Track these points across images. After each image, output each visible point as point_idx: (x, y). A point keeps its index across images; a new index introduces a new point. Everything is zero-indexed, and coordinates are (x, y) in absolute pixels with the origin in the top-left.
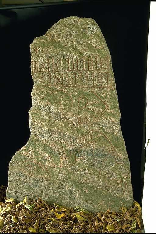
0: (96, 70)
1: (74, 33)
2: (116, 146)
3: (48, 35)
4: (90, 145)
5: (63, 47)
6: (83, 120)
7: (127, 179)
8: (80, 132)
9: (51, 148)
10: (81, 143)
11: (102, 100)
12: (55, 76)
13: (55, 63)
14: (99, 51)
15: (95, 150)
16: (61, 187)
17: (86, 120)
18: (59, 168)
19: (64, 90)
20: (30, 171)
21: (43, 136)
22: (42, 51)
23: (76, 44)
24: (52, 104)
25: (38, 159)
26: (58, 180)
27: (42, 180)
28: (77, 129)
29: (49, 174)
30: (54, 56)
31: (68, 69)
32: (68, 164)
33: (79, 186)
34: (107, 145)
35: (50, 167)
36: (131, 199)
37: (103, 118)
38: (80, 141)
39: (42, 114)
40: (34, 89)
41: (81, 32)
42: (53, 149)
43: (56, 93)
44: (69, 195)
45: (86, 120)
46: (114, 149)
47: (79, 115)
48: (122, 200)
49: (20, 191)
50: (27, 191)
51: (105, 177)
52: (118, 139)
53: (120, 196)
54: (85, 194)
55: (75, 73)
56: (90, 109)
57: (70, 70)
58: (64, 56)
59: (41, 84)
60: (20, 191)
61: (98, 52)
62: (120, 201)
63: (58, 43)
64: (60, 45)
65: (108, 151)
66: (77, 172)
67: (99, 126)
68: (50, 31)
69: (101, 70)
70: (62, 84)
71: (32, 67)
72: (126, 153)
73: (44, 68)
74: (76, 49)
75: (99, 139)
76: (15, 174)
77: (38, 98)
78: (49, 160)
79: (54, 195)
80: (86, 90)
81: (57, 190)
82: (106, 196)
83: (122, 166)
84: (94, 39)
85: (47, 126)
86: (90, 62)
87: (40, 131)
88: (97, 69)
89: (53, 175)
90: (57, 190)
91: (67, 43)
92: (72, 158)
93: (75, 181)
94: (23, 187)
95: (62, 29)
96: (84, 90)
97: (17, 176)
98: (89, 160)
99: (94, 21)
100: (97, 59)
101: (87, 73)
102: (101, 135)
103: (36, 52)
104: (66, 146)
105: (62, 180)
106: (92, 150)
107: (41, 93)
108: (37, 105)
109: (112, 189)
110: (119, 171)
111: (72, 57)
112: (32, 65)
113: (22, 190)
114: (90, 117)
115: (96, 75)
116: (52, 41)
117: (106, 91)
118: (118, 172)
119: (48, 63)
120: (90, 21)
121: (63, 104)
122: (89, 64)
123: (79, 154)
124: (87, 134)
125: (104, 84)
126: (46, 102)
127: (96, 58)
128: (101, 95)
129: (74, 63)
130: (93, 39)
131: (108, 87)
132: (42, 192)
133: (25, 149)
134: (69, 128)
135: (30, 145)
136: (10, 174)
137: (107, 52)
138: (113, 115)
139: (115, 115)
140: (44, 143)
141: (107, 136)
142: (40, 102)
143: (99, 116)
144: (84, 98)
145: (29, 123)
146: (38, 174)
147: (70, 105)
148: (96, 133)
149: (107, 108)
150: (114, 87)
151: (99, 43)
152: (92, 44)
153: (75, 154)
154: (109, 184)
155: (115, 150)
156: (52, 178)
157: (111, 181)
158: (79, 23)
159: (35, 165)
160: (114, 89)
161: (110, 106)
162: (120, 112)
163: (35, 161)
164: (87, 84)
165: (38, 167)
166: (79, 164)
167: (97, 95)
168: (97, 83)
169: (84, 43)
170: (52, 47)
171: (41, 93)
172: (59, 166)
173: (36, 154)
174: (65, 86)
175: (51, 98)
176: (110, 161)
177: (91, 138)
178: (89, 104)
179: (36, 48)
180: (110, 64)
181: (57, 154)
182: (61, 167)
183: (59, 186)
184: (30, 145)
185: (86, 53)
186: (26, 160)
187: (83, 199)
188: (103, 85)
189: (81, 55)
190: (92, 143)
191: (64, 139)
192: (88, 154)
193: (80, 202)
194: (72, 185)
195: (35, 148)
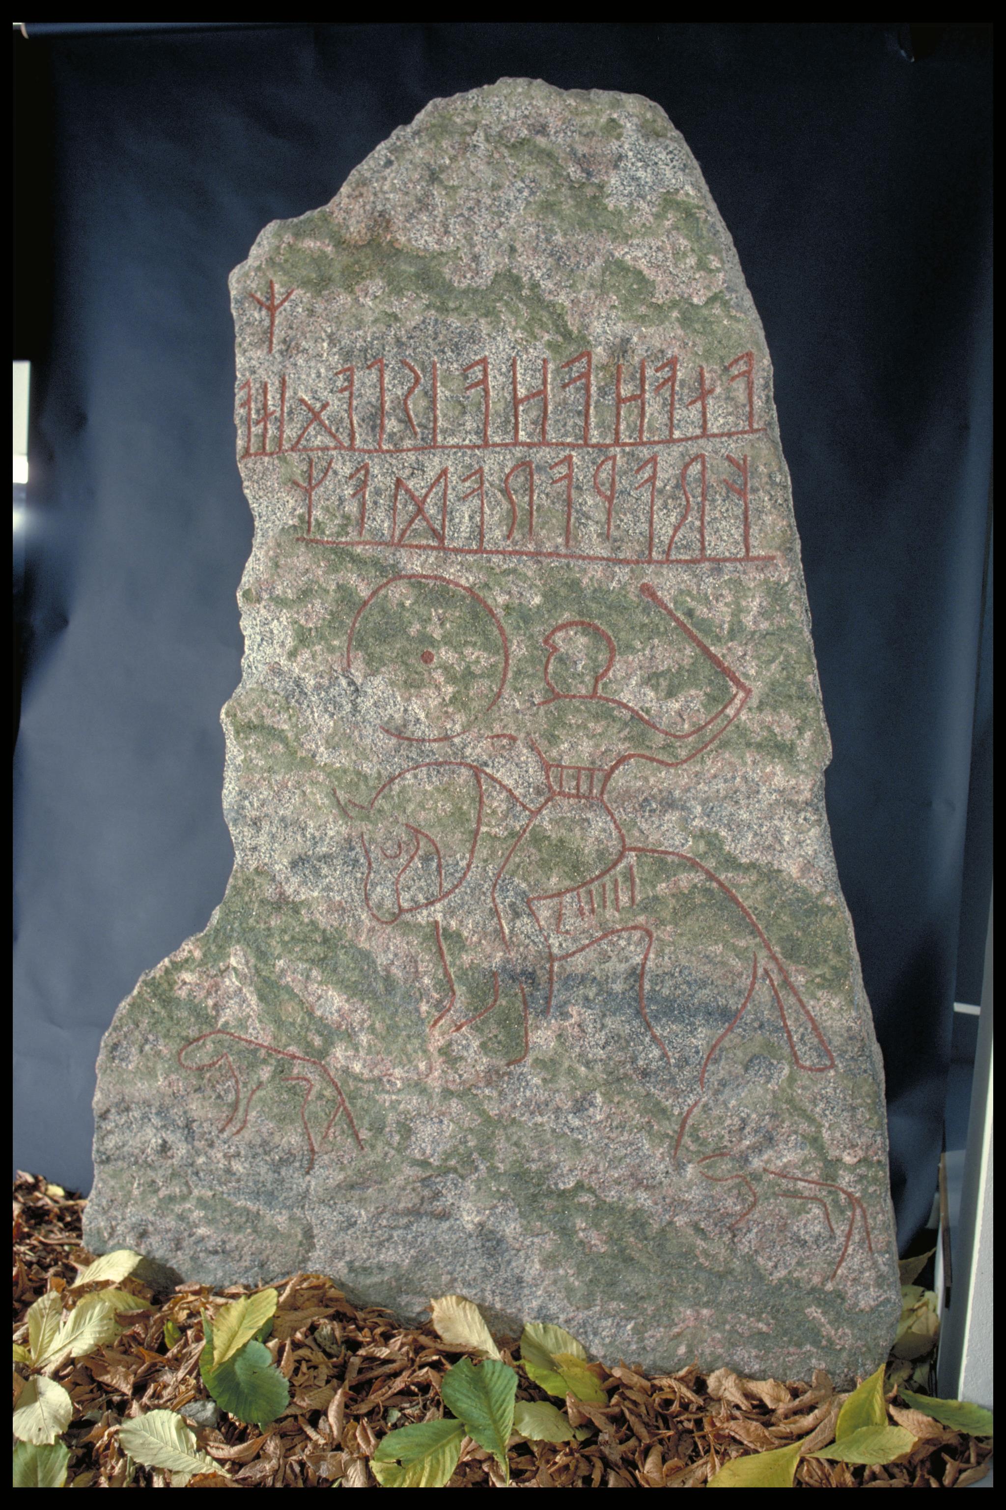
0: (670, 441)
1: (520, 191)
2: (792, 950)
3: (348, 207)
4: (623, 943)
5: (449, 288)
6: (578, 780)
7: (862, 1170)
8: (560, 854)
9: (366, 956)
10: (557, 929)
11: (705, 650)
12: (390, 481)
13: (395, 391)
14: (689, 316)
15: (658, 979)
16: (428, 1208)
17: (599, 775)
18: (419, 1087)
19: (450, 572)
20: (231, 1098)
21: (317, 872)
22: (311, 312)
23: (532, 266)
24: (373, 665)
25: (279, 1023)
26: (415, 1163)
27: (312, 1162)
28: (538, 838)
29: (351, 1124)
30: (390, 351)
31: (482, 433)
32: (476, 1060)
33: (549, 1204)
34: (734, 948)
35: (357, 1078)
36: (888, 1300)
37: (712, 766)
38: (559, 917)
39: (307, 729)
40: (255, 567)
41: (571, 188)
42: (382, 960)
43: (399, 593)
44: (482, 1262)
45: (599, 775)
46: (781, 970)
47: (553, 740)
48: (832, 1302)
49: (170, 1222)
50: (210, 1222)
51: (720, 1153)
52: (808, 908)
53: (816, 1280)
54: (586, 1258)
55: (524, 465)
56: (626, 706)
57: (495, 445)
58: (457, 348)
59: (303, 533)
60: (170, 1222)
61: (685, 321)
62: (814, 1312)
63: (415, 257)
64: (427, 277)
65: (745, 982)
66: (532, 1113)
67: (684, 823)
68: (364, 182)
69: (701, 442)
70: (441, 538)
71: (247, 421)
72: (861, 997)
73: (321, 423)
74: (537, 300)
75: (685, 904)
76: (137, 1114)
77: (281, 627)
78: (350, 1036)
79: (388, 1256)
80: (599, 575)
81: (407, 1227)
82: (721, 1276)
83: (830, 1084)
84: (654, 234)
85: (344, 812)
86: (626, 391)
87: (297, 844)
88: (677, 434)
89: (378, 1129)
90: (407, 1227)
91: (476, 258)
92: (504, 1022)
93: (520, 1176)
94: (184, 1198)
95: (443, 169)
96: (585, 581)
97: (150, 1131)
98: (615, 1037)
99: (659, 116)
100: (674, 371)
101: (608, 465)
102: (697, 878)
103: (267, 323)
104: (463, 948)
105: (435, 1161)
106: (636, 974)
107: (305, 594)
108: (276, 670)
109: (764, 1231)
110: (811, 1120)
111: (509, 352)
112: (246, 404)
113: (181, 1218)
114: (622, 760)
115: (666, 473)
116: (373, 244)
117: (737, 585)
118: (804, 1126)
119: (346, 394)
120: (633, 111)
121: (446, 668)
122: (522, 401)
123: (548, 999)
124: (603, 873)
125: (724, 538)
126: (331, 650)
127: (672, 363)
128: (702, 611)
129: (522, 392)
130: (647, 231)
131: (747, 558)
132: (309, 1234)
133: (197, 954)
134: (484, 829)
135: (232, 930)
136: (104, 1116)
137: (745, 324)
138: (782, 750)
139: (792, 747)
140: (322, 922)
141: (738, 886)
142: (292, 655)
143: (683, 753)
144: (587, 628)
145: (225, 791)
146: (282, 1119)
147: (490, 673)
148: (662, 863)
149: (743, 702)
150: (790, 562)
151: (691, 261)
152: (642, 265)
153: (525, 1003)
154: (744, 1200)
155: (786, 983)
156: (373, 1147)
157: (757, 1177)
158: (553, 124)
159: (265, 1061)
160: (789, 573)
161: (758, 688)
162: (824, 725)
163: (260, 1033)
164: (605, 536)
165: (281, 1071)
166: (549, 1066)
167: (670, 613)
168: (676, 529)
169: (591, 259)
170: (376, 285)
171: (305, 594)
172: (421, 1078)
173: (269, 990)
174: (457, 551)
175: (367, 631)
176: (757, 1050)
177: (632, 899)
178: (618, 669)
179: (271, 296)
180: (763, 402)
181: (407, 996)
182: (434, 1083)
183: (417, 1200)
184: (232, 930)
185: (604, 327)
186: (206, 1030)
187: (570, 1290)
188: (717, 546)
189: (572, 345)
190: (635, 928)
191: (455, 898)
192: (610, 1004)
193: (553, 1308)
194: (504, 1197)
195: (262, 955)
